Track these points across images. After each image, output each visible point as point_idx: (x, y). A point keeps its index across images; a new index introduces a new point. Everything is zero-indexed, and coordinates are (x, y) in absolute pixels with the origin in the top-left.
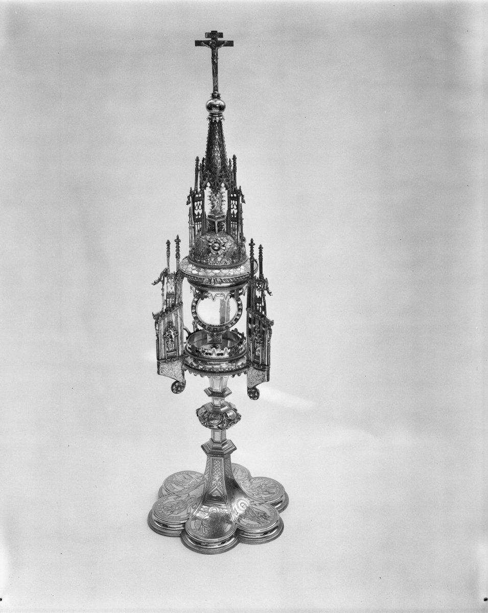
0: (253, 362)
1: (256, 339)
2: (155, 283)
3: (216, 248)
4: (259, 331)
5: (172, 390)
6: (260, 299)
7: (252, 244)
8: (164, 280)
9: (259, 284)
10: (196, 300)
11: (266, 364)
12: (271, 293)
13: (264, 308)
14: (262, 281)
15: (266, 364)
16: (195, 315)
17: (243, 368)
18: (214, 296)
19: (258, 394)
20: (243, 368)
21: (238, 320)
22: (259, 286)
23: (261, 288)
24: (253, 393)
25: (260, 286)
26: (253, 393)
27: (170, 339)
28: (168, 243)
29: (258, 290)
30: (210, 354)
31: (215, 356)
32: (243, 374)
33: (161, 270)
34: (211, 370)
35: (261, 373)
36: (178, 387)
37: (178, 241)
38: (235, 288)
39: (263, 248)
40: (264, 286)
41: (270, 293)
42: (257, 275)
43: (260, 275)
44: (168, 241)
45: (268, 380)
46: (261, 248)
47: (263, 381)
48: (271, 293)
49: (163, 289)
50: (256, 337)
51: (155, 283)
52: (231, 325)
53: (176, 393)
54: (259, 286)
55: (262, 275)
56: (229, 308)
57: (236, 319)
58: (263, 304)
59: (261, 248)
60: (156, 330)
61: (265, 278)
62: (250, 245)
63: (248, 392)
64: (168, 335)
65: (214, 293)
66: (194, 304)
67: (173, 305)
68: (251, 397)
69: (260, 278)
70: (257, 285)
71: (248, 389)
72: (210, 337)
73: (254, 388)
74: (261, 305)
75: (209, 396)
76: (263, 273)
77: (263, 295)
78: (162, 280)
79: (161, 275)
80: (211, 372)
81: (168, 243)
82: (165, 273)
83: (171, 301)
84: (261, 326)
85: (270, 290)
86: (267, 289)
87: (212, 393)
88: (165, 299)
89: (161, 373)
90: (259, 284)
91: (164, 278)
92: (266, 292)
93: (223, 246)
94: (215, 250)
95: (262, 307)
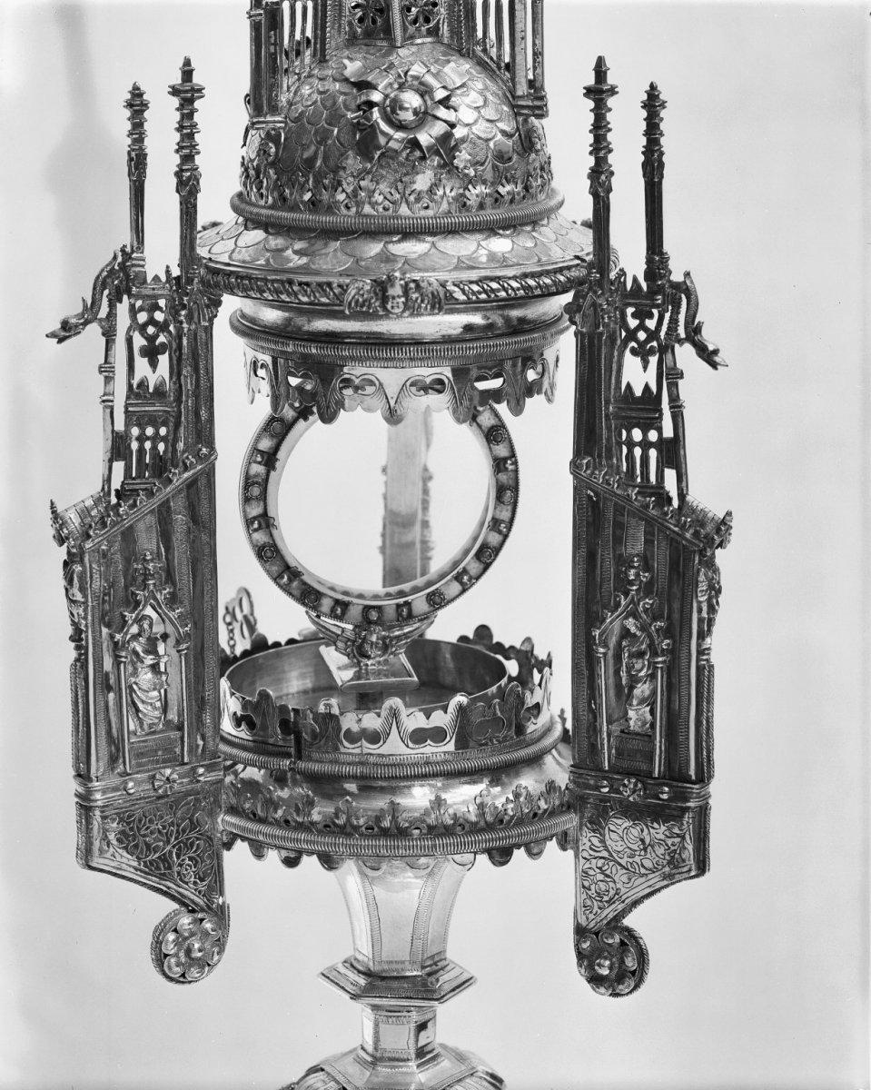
0: (613, 769)
1: (626, 633)
2: (67, 331)
3: (408, 116)
4: (650, 583)
5: (160, 959)
6: (650, 400)
7: (599, 92)
8: (112, 315)
9: (642, 315)
10: (266, 444)
11: (692, 772)
12: (716, 352)
13: (672, 453)
14: (664, 289)
15: (692, 772)
16: (260, 537)
17: (552, 813)
18: (392, 391)
19: (642, 957)
20: (552, 813)
21: (497, 550)
22: (642, 327)
23: (653, 335)
24: (611, 957)
25: (651, 324)
26: (611, 957)
27: (149, 660)
28: (137, 104)
29: (634, 352)
30: (375, 737)
31: (402, 749)
32: (552, 846)
33: (101, 258)
34: (386, 823)
35: (660, 831)
36: (187, 952)
37: (187, 94)
38: (489, 366)
39: (663, 105)
40: (674, 321)
41: (708, 356)
42: (630, 258)
43: (649, 261)
44: (136, 88)
45: (702, 866)
46: (653, 103)
47: (671, 879)
48: (716, 352)
49: (107, 370)
50: (631, 624)
51: (67, 331)
52: (456, 587)
53: (182, 979)
54: (642, 327)
55: (664, 259)
56: (79, 775)
57: (484, 546)
58: (668, 432)
59: (653, 103)
60: (72, 601)
61: (677, 277)
62: (175, 91)
63: (580, 955)
64: (135, 637)
65: (391, 377)
66: (257, 469)
67: (162, 442)
68: (596, 980)
69: (651, 274)
70: (633, 323)
71: (580, 932)
72: (345, 660)
73: (615, 924)
74: (653, 436)
75: (354, 997)
76: (668, 246)
77: (670, 375)
78: (103, 312)
79: (100, 284)
80: (385, 833)
81: (137, 104)
82: (121, 278)
83: (150, 441)
84: (647, 560)
85: (710, 337)
86: (694, 333)
87: (378, 983)
88: (120, 425)
89: (97, 861)
90: (642, 315)
91: (112, 306)
92: (685, 355)
93: (445, 102)
94: (400, 126)
95: (662, 444)
